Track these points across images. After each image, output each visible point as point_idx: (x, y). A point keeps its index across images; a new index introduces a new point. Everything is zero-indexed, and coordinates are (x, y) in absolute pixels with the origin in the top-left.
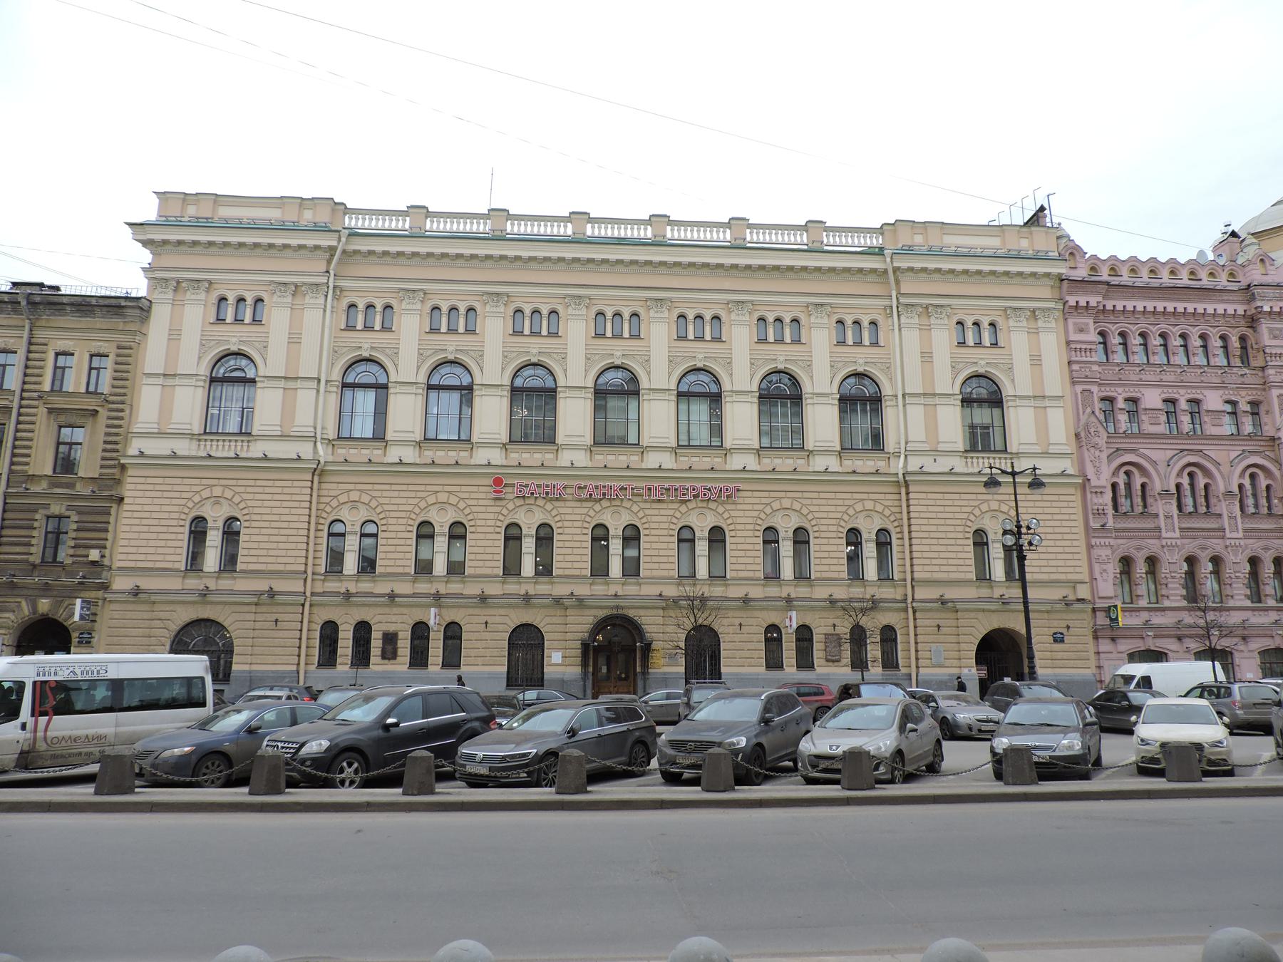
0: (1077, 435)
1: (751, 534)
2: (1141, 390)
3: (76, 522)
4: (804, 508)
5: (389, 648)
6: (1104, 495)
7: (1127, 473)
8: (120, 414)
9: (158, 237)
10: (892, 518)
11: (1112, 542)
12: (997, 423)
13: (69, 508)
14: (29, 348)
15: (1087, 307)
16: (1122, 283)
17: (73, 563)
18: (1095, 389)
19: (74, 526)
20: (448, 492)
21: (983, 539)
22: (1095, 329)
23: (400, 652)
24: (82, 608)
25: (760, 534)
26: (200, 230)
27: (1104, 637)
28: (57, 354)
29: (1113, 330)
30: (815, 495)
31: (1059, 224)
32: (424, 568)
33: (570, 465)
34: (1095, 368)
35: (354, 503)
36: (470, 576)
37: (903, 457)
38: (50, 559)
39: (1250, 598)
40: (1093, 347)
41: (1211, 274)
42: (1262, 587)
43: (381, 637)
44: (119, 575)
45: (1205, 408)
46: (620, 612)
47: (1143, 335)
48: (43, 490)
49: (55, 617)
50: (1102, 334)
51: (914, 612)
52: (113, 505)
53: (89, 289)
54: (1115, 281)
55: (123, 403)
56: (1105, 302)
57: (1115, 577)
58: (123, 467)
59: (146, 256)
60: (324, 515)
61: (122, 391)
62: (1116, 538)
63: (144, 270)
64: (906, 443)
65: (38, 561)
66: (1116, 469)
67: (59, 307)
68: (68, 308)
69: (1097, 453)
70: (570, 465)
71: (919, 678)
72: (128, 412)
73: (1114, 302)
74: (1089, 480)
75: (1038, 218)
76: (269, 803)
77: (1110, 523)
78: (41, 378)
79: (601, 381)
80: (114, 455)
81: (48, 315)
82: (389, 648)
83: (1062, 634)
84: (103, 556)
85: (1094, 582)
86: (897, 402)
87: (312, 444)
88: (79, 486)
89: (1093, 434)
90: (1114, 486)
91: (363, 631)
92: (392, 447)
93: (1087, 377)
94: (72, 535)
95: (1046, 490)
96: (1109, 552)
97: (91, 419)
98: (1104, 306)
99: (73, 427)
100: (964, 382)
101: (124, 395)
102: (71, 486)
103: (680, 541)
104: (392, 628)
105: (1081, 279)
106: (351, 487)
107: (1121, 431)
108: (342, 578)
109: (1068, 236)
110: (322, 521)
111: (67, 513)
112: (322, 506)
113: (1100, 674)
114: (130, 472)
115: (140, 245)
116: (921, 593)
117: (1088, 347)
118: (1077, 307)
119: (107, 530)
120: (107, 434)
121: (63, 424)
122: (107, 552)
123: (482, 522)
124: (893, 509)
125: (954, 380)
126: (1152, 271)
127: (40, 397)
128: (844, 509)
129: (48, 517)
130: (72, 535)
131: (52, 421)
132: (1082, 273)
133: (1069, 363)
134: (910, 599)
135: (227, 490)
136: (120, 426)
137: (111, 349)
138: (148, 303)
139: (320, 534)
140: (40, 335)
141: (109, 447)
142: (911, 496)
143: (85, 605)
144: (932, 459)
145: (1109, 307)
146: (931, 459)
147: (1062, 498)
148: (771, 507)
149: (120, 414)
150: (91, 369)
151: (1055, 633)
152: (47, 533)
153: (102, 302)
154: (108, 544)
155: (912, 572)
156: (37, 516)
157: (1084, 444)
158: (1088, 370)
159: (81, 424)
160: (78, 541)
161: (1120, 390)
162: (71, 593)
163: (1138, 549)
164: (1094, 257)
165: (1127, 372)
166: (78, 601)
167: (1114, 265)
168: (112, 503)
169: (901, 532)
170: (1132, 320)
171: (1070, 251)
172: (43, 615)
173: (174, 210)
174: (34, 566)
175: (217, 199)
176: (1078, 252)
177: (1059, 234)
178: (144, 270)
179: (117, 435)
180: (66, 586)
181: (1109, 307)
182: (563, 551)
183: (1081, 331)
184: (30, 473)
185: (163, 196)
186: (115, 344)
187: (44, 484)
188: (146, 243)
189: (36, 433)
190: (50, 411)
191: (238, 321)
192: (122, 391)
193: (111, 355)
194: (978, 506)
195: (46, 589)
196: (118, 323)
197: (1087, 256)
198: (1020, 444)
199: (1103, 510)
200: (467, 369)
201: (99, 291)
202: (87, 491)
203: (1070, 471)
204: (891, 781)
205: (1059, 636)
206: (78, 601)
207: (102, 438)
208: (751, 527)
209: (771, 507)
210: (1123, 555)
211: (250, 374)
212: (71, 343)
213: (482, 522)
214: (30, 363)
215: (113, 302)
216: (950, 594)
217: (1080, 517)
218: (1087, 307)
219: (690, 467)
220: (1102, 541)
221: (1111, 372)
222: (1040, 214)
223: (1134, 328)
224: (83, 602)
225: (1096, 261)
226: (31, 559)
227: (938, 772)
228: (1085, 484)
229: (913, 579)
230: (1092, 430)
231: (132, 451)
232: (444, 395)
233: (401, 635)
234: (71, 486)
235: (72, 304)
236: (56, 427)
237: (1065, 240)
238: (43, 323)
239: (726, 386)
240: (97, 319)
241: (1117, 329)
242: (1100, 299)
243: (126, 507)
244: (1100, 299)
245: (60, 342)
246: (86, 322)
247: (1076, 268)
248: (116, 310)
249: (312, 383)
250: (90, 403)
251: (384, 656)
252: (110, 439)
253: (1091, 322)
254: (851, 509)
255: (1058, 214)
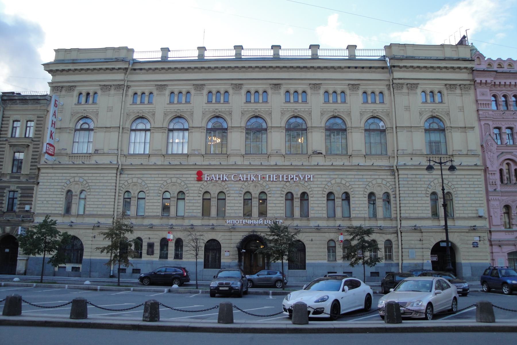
0: (482, 146)
1: (321, 196)
2: (514, 123)
3: (20, 193)
4: (384, 181)
5: (150, 250)
6: (495, 175)
7: (508, 164)
8: (38, 146)
9: (54, 68)
10: (391, 187)
11: (500, 198)
12: (442, 140)
13: (18, 187)
14: (2, 119)
15: (486, 83)
16: (504, 71)
17: (19, 211)
18: (490, 123)
19: (20, 195)
20: (382, 179)
21: (450, 197)
22: (490, 94)
23: (155, 252)
24: (21, 231)
25: (201, 195)
26: (258, 62)
27: (495, 245)
28: (14, 121)
29: (500, 94)
30: (61, 175)
31: (472, 44)
32: (332, 216)
33: (180, 164)
34: (490, 113)
35: (379, 184)
36: (312, 217)
37: (396, 158)
38: (11, 209)
39: (505, 225)
40: (489, 102)
41: (509, 65)
42: (511, 220)
43: (147, 245)
44: (492, 223)
45: (515, 131)
46: (255, 233)
47: (505, 96)
48: (8, 180)
49: (12, 235)
50: (494, 96)
51: (401, 233)
52: (35, 186)
53: (27, 93)
54: (500, 70)
55: (39, 141)
56: (495, 81)
57: (502, 215)
58: (39, 169)
59: (49, 77)
60: (122, 189)
61: (39, 136)
62: (502, 196)
63: (49, 83)
64: (397, 151)
65: (6, 210)
66: (502, 162)
67: (14, 101)
68: (18, 101)
69: (492, 154)
70: (180, 164)
71: (403, 266)
72: (41, 145)
73: (500, 81)
74: (488, 168)
75: (463, 41)
76: (303, 329)
77: (499, 189)
78: (7, 132)
79: (326, 124)
80: (36, 164)
81: (10, 105)
82: (150, 250)
83: (477, 243)
84: (31, 208)
85: (491, 217)
86: (393, 131)
87: (117, 156)
88: (21, 178)
89: (490, 145)
90: (501, 171)
91: (179, 243)
92: (192, 157)
93: (486, 117)
94: (19, 199)
95: (457, 172)
96: (498, 203)
97: (27, 148)
98: (495, 83)
99: (19, 152)
100: (426, 121)
101: (40, 138)
102: (19, 178)
103: (286, 200)
104: (151, 241)
105: (483, 70)
106: (173, 176)
107: (504, 143)
108: (210, 218)
109: (476, 49)
110: (121, 192)
111: (17, 190)
112: (121, 185)
113: (493, 263)
114: (42, 171)
115: (48, 72)
116: (405, 223)
117: (487, 103)
118: (481, 83)
119: (32, 197)
120: (33, 155)
121: (15, 151)
122: (33, 207)
123: (192, 192)
124: (391, 183)
125: (361, 120)
126: (509, 65)
127: (6, 140)
128: (325, 183)
129: (10, 191)
130: (19, 199)
131: (11, 150)
132: (484, 67)
133: (478, 110)
134: (399, 227)
135: (80, 178)
136: (38, 151)
137: (35, 118)
138: (50, 98)
139: (120, 198)
140: (7, 113)
141: (33, 160)
142: (400, 176)
143: (23, 229)
144: (409, 158)
145: (497, 83)
146: (409, 158)
147: (94, 175)
148: (331, 183)
149: (38, 146)
150: (27, 127)
151: (473, 243)
152: (9, 198)
153: (31, 98)
154: (33, 203)
155: (400, 214)
156: (5, 191)
157: (485, 150)
158: (487, 114)
159: (23, 151)
160: (21, 202)
161: (503, 123)
162: (17, 224)
163: (513, 201)
164: (490, 59)
165: (507, 115)
166: (20, 228)
167: (500, 63)
168: (34, 185)
169: (395, 194)
170: (509, 89)
171: (477, 56)
172: (7, 234)
173: (61, 58)
174: (4, 213)
175: (78, 50)
176: (481, 56)
177: (472, 48)
178: (49, 83)
179: (37, 155)
180: (16, 221)
181: (497, 83)
182: (190, 204)
183: (483, 94)
184: (2, 173)
185: (56, 51)
186: (36, 116)
187: (8, 177)
188: (50, 71)
189: (5, 155)
190: (11, 146)
191: (142, 103)
192: (39, 136)
193: (35, 121)
194: (433, 181)
195: (8, 222)
196: (38, 106)
197: (486, 59)
198: (353, 151)
199: (495, 182)
200: (264, 120)
201: (31, 93)
202: (24, 180)
203: (479, 164)
204: (426, 319)
205: (475, 244)
206: (20, 228)
207: (31, 157)
208: (197, 192)
209: (331, 183)
210: (505, 204)
211: (225, 126)
212: (19, 116)
213: (192, 192)
214: (3, 126)
215: (35, 98)
216: (419, 223)
217: (483, 186)
218: (486, 83)
219: (358, 164)
220: (495, 197)
221: (499, 115)
222: (463, 40)
223: (510, 93)
224: (22, 228)
225: (511, 61)
226: (3, 209)
227: (369, 311)
228: (486, 170)
229: (400, 217)
230: (489, 143)
231: (42, 162)
232: (138, 133)
233: (155, 244)
234: (19, 178)
235: (19, 100)
236: (13, 153)
237: (475, 51)
238: (8, 108)
239: (349, 125)
240: (29, 105)
241: (501, 94)
242: (492, 79)
243: (40, 187)
244: (492, 79)
245: (15, 116)
246: (25, 107)
247: (480, 64)
248: (37, 101)
249: (117, 129)
250: (26, 142)
251: (148, 254)
252: (34, 157)
253: (488, 90)
254: (432, 183)
255: (470, 40)
